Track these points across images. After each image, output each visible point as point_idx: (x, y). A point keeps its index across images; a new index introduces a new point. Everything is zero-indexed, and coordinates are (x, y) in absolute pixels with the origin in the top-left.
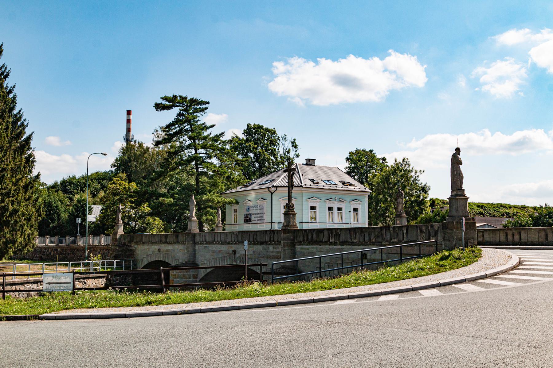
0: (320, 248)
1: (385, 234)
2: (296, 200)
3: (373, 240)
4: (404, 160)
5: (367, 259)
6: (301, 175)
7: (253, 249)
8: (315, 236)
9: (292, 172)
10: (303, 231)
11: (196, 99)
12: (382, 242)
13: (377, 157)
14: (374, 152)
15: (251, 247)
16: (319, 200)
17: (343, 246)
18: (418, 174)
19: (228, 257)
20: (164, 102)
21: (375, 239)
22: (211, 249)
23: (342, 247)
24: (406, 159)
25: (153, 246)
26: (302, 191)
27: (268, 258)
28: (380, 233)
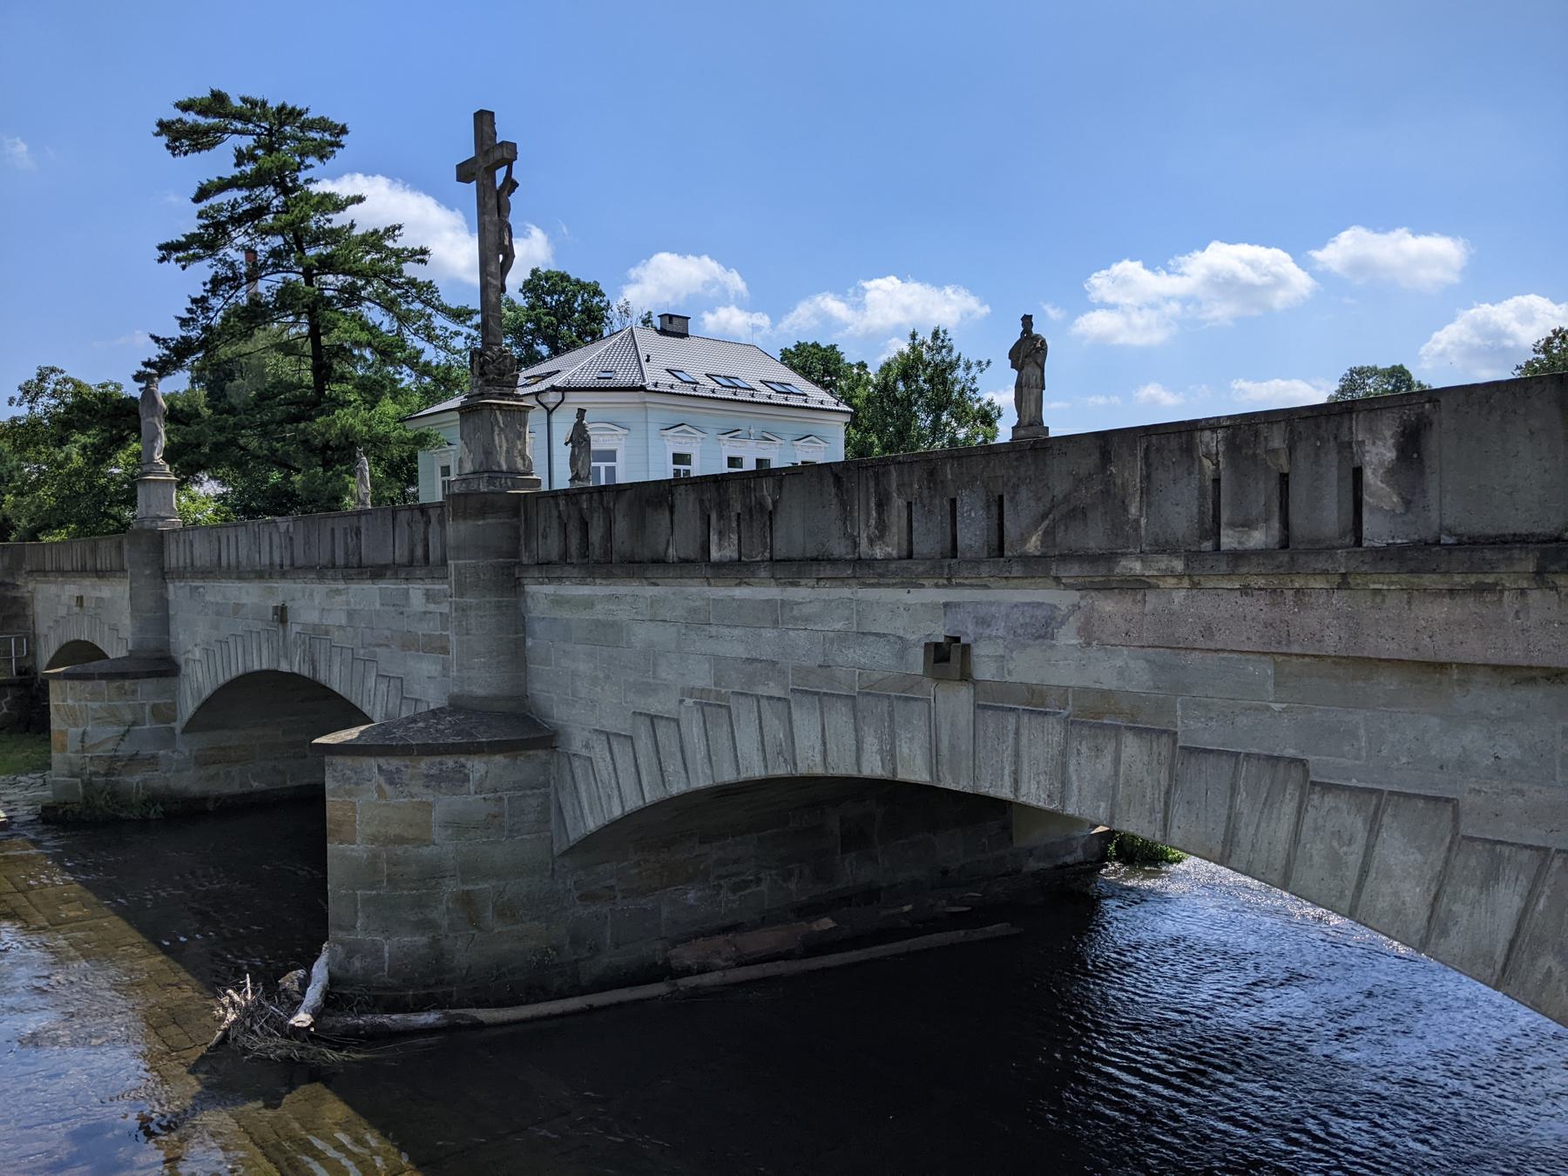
0: (654, 602)
1: (1146, 492)
2: (626, 432)
3: (1024, 539)
4: (935, 335)
5: (975, 683)
6: (643, 358)
7: (348, 603)
8: (621, 527)
9: (500, 174)
10: (562, 503)
11: (294, 109)
12: (1110, 557)
13: (847, 361)
14: (838, 349)
15: (338, 592)
16: (699, 435)
17: (795, 584)
18: (974, 370)
19: (264, 636)
20: (191, 117)
21: (1049, 534)
22: (212, 599)
23: (792, 593)
24: (941, 332)
25: (67, 587)
26: (645, 402)
27: (405, 647)
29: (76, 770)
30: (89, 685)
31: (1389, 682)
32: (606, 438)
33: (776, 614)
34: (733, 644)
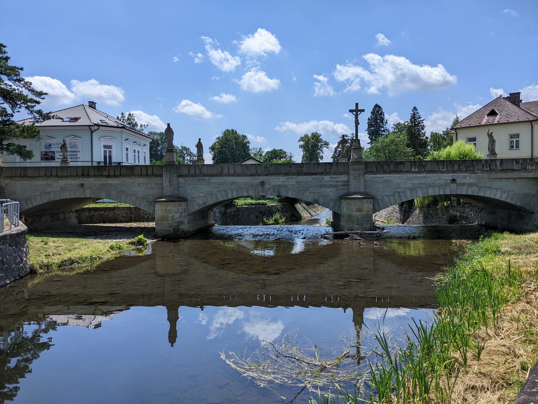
0: (399, 177)
18: (143, 127)
28: (472, 164)
29: (171, 225)
30: (174, 203)
31: (498, 180)
32: (109, 141)
33: (425, 178)
34: (416, 182)
